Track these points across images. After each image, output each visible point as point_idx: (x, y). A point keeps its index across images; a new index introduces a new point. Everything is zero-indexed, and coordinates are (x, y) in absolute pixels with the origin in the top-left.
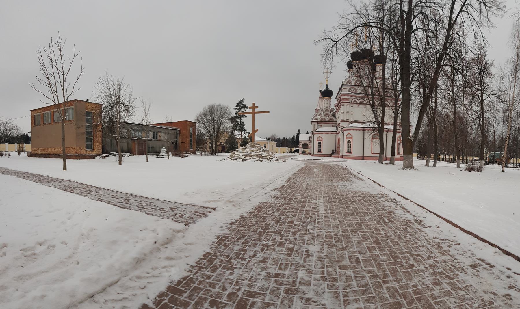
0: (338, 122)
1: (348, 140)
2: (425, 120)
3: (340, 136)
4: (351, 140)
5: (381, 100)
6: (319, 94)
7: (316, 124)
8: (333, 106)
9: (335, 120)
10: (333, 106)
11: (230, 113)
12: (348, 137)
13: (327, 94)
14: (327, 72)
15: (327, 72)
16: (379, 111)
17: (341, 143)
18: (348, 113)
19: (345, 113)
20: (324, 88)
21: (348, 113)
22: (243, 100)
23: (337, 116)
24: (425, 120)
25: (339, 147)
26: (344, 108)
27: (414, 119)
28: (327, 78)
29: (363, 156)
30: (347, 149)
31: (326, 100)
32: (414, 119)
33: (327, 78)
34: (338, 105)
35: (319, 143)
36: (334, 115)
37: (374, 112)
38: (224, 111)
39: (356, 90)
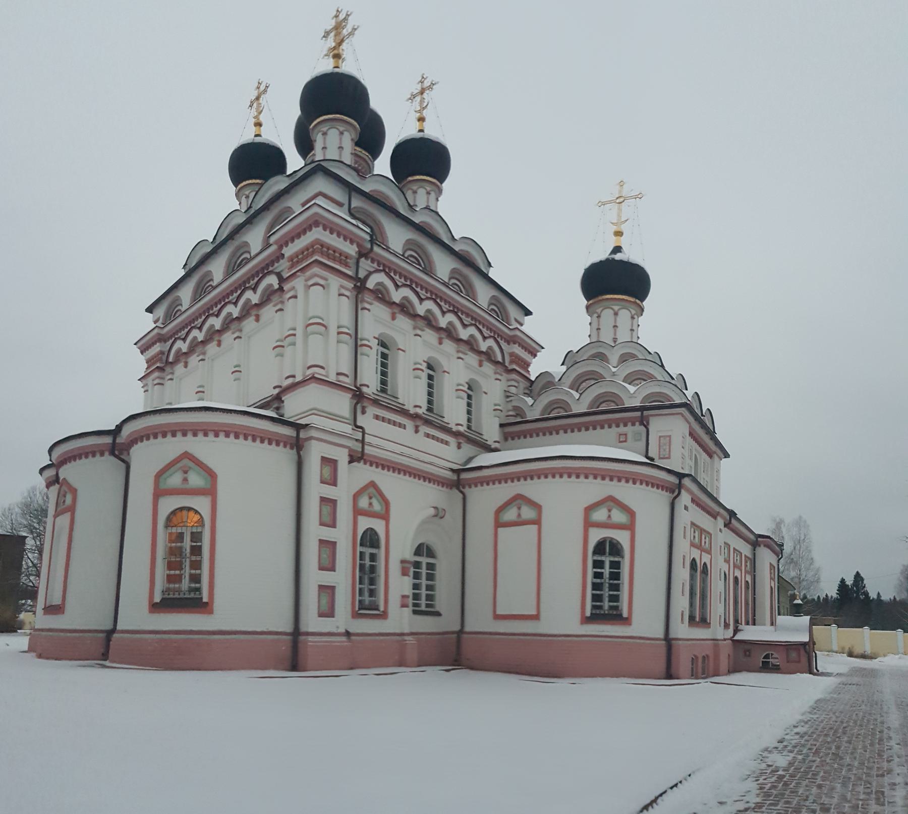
29: (296, 633)
30: (161, 571)
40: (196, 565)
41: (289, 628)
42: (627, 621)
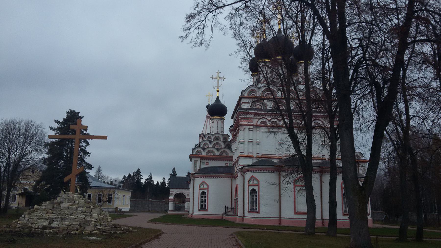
0: (235, 158)
1: (251, 188)
2: (387, 148)
3: (239, 181)
4: (256, 188)
5: (304, 117)
6: (205, 112)
7: (198, 160)
8: (226, 131)
9: (230, 154)
10: (226, 131)
11: (42, 134)
12: (251, 183)
13: (216, 110)
14: (218, 78)
15: (218, 78)
16: (302, 137)
17: (240, 193)
18: (251, 143)
19: (246, 143)
20: (212, 102)
21: (251, 143)
22: (174, 170)
23: (234, 147)
24: (387, 148)
25: (236, 201)
26: (244, 135)
27: (363, 142)
28: (218, 86)
31: (215, 122)
32: (363, 142)
33: (218, 86)
34: (235, 129)
35: (203, 193)
36: (229, 146)
37: (294, 138)
38: (33, 131)
39: (264, 104)
40: (205, 202)
41: (277, 216)
42: (258, 213)
